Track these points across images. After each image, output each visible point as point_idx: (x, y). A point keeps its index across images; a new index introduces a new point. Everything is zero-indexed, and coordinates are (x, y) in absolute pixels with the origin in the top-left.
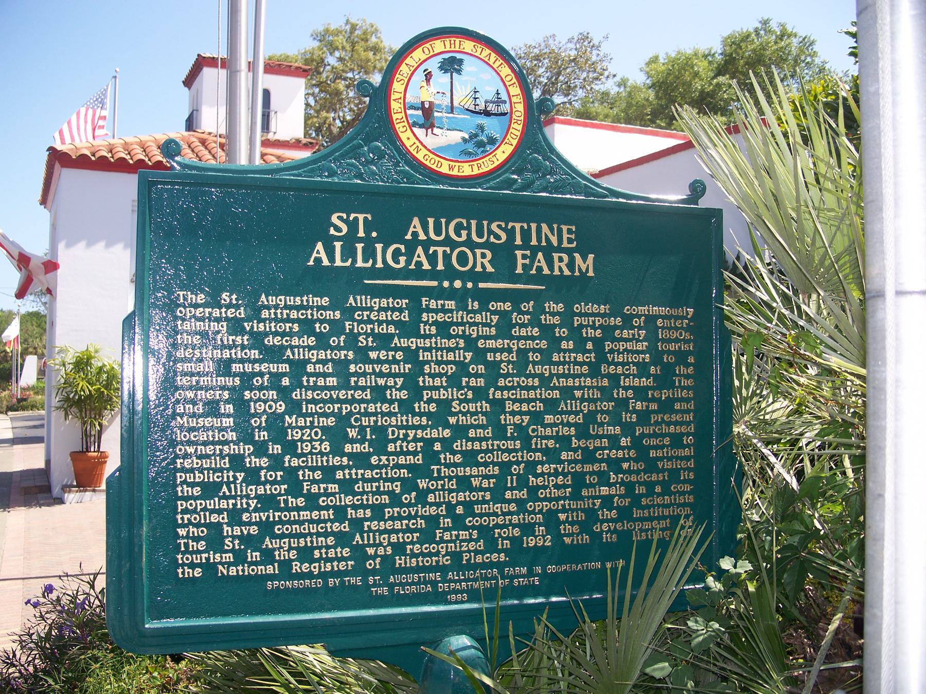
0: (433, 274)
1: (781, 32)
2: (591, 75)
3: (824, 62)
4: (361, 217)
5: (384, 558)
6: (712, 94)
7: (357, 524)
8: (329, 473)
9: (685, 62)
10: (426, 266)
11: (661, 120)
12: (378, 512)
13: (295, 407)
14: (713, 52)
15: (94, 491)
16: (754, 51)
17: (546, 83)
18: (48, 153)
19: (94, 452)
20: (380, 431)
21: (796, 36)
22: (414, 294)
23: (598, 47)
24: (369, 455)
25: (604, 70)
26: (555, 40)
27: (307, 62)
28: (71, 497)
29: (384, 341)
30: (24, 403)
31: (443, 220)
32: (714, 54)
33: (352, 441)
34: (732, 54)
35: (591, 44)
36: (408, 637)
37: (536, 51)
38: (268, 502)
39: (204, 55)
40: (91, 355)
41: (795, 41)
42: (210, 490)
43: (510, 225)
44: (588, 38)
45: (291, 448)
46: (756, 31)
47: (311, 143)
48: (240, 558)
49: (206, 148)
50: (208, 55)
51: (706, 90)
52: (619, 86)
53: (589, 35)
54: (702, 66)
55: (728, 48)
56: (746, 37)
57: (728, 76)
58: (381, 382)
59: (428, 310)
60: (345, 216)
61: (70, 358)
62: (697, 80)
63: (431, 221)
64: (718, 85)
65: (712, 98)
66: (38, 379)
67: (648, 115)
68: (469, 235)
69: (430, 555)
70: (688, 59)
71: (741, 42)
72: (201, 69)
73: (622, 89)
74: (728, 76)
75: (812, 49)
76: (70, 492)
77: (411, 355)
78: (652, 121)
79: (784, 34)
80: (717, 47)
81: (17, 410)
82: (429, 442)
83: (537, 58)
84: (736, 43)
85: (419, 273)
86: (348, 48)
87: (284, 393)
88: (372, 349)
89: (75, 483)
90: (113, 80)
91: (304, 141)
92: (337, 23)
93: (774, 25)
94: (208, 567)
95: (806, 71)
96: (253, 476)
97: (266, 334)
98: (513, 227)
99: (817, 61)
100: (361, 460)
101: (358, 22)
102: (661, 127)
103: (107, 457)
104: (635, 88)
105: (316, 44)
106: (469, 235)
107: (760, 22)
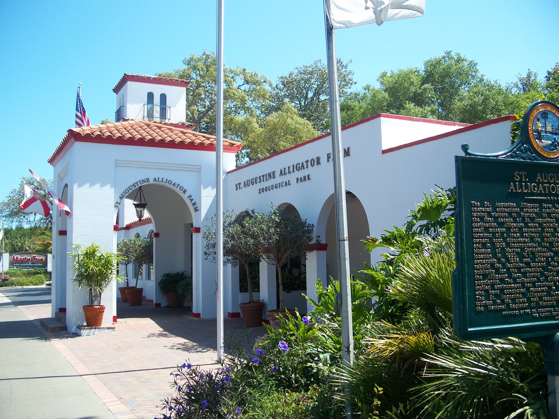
0: (545, 195)
1: (457, 58)
2: (343, 83)
3: (483, 76)
4: (523, 173)
5: (536, 302)
6: (421, 94)
7: (528, 289)
8: (519, 269)
9: (405, 76)
10: (543, 192)
11: (393, 109)
12: (534, 283)
13: (508, 244)
14: (418, 70)
15: (98, 328)
16: (444, 69)
17: (316, 88)
18: (68, 133)
19: (97, 305)
20: (533, 253)
21: (466, 61)
22: (540, 202)
23: (346, 67)
24: (530, 263)
25: (350, 80)
26: (321, 63)
27: (181, 77)
28: (84, 332)
29: (532, 219)
30: (7, 282)
31: (547, 174)
32: (419, 71)
33: (525, 258)
34: (431, 71)
35: (342, 65)
36: (544, 333)
37: (310, 69)
38: (502, 281)
39: (128, 74)
40: (95, 249)
41: (466, 64)
42: (485, 276)
43: (521, 173)
44: (340, 61)
45: (508, 260)
46: (444, 57)
47: (191, 125)
48: (495, 303)
49: (150, 128)
50: (130, 74)
51: (418, 92)
52: (365, 89)
53: (341, 60)
54: (415, 79)
55: (428, 68)
56: (439, 62)
57: (430, 84)
58: (532, 234)
59: (545, 208)
60: (518, 173)
61: (82, 251)
62: (412, 86)
63: (543, 174)
64: (425, 89)
65: (422, 97)
66: (9, 267)
67: (385, 107)
68: (554, 180)
69: (550, 301)
70: (407, 75)
71: (436, 64)
72: (126, 82)
73: (367, 91)
74: (430, 84)
75: (476, 68)
76: (84, 329)
77: (541, 225)
78: (388, 111)
79: (459, 60)
80: (422, 68)
81: (2, 287)
82: (547, 258)
83: (311, 73)
84: (432, 66)
85: (541, 195)
86: (205, 69)
87: (505, 239)
88: (529, 223)
89: (85, 324)
90: (78, 89)
91: (187, 124)
92: (198, 54)
93: (453, 54)
94: (485, 306)
95: (472, 80)
96: (497, 271)
97: (498, 217)
98: (522, 174)
99: (479, 75)
100: (528, 264)
101: (210, 54)
102: (392, 113)
103: (104, 309)
104: (378, 91)
105: (186, 67)
106: (554, 180)
107: (445, 53)
